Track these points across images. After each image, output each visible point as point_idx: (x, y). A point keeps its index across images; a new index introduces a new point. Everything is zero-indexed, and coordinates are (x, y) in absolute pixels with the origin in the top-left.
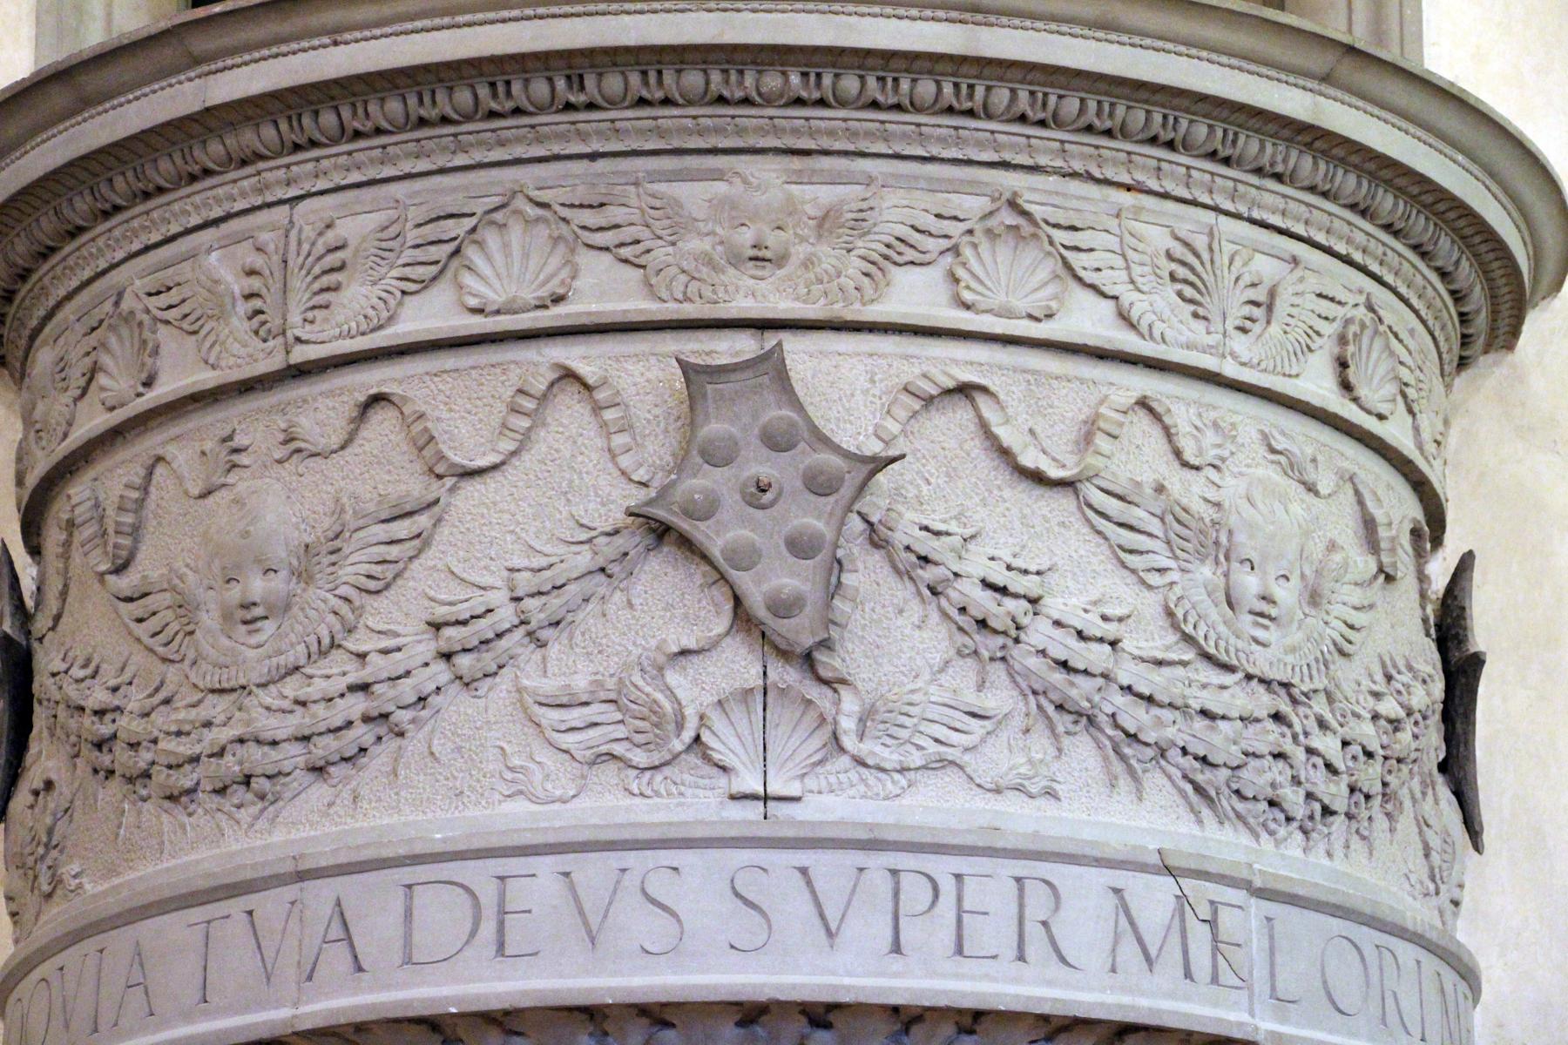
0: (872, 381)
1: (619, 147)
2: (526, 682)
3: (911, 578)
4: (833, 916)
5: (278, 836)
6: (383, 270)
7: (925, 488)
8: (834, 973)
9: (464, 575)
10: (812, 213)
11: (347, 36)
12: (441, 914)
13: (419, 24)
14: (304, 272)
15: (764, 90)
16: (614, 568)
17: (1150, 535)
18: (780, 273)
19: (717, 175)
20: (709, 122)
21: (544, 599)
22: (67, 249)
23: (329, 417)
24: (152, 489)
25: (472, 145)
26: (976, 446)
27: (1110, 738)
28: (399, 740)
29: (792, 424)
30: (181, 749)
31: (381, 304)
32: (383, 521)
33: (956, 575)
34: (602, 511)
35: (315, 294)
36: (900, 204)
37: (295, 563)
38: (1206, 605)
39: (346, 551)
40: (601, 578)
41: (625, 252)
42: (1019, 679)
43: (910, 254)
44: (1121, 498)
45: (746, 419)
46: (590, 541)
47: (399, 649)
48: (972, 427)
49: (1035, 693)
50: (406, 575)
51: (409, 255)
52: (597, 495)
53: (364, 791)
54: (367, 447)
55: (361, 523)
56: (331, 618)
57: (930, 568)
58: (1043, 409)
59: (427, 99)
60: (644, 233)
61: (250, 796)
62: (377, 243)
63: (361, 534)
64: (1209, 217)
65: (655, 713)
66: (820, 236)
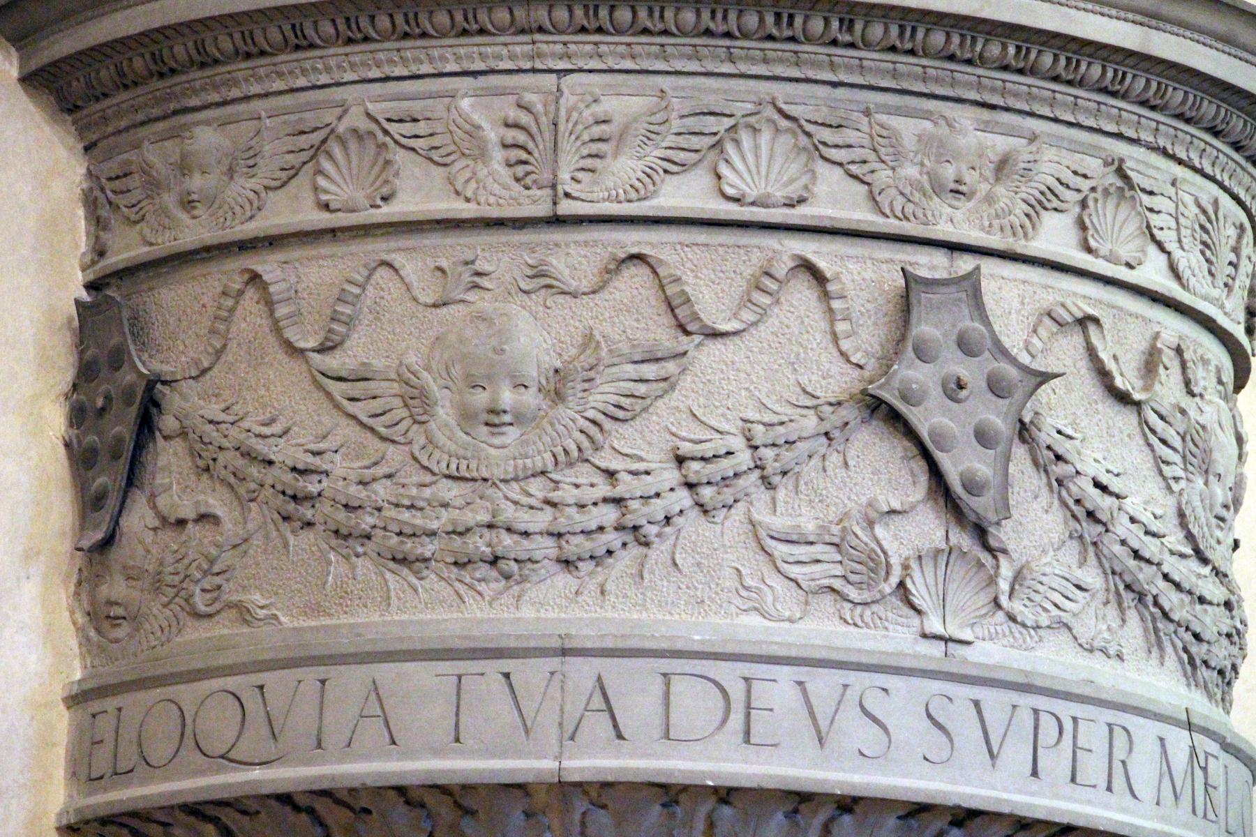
1: (860, 81)
2: (756, 517)
3: (1046, 471)
5: (527, 612)
6: (648, 149)
7: (1052, 396)
8: (994, 788)
9: (703, 419)
10: (993, 158)
12: (694, 702)
14: (573, 137)
15: (987, 55)
16: (835, 434)
18: (970, 205)
19: (927, 115)
21: (776, 450)
23: (580, 263)
24: (369, 288)
25: (741, 58)
26: (1083, 365)
27: (1152, 614)
28: (644, 550)
29: (983, 337)
32: (636, 362)
33: (1078, 472)
34: (824, 383)
35: (583, 158)
37: (544, 382)
39: (598, 381)
40: (824, 440)
41: (854, 169)
42: (1104, 560)
43: (1056, 203)
44: (1162, 418)
45: (947, 326)
46: (815, 407)
47: (647, 473)
48: (1082, 350)
49: (1114, 573)
50: (651, 410)
51: (671, 140)
52: (819, 369)
53: (610, 586)
54: (617, 295)
55: (616, 360)
56: (578, 435)
57: (1060, 464)
58: (1127, 333)
60: (871, 156)
61: (494, 574)
62: (647, 126)
63: (614, 370)
65: (872, 560)
66: (998, 179)
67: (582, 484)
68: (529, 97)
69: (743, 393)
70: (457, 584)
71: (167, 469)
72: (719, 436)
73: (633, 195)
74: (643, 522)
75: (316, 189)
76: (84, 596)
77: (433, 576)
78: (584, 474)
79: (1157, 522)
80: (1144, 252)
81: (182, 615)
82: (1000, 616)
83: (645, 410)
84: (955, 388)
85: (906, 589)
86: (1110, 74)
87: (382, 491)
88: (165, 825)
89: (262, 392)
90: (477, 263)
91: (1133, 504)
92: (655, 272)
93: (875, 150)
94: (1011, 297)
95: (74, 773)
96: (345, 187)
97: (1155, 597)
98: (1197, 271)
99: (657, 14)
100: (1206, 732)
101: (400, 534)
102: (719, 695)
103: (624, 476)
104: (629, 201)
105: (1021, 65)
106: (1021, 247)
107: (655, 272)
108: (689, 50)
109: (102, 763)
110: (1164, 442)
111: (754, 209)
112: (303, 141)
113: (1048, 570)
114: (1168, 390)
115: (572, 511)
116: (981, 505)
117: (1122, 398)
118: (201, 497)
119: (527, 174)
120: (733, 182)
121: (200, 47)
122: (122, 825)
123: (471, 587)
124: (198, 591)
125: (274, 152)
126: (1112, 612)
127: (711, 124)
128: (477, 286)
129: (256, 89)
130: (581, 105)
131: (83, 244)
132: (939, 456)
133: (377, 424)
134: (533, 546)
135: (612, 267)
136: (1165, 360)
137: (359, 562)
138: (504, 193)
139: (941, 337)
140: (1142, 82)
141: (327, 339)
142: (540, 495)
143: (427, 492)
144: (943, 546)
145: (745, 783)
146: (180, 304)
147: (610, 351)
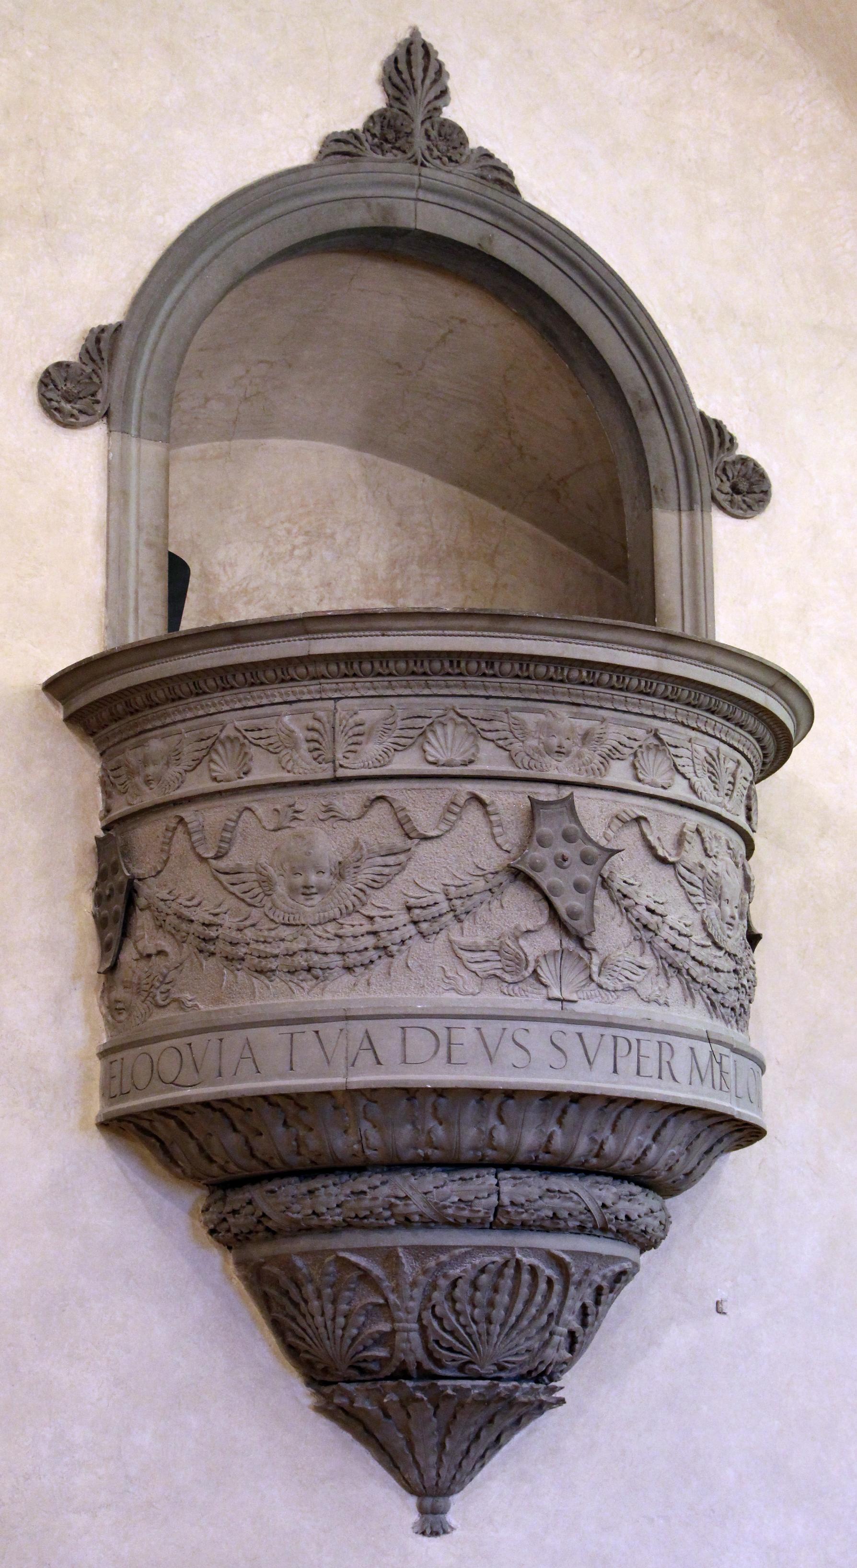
0: (601, 811)
2: (453, 938)
3: (618, 904)
4: (591, 1055)
5: (328, 997)
6: (385, 738)
7: (621, 862)
11: (389, 633)
12: (420, 1042)
13: (426, 632)
15: (571, 677)
16: (495, 890)
17: (698, 887)
18: (567, 759)
19: (541, 711)
20: (543, 688)
21: (462, 900)
22: (191, 700)
24: (240, 822)
26: (639, 844)
28: (390, 959)
30: (268, 950)
31: (384, 755)
36: (615, 734)
37: (333, 869)
38: (713, 917)
39: (362, 867)
40: (489, 893)
41: (500, 742)
43: (618, 755)
44: (689, 870)
46: (483, 876)
47: (391, 917)
48: (638, 836)
49: (661, 958)
51: (398, 733)
53: (373, 980)
55: (371, 855)
57: (626, 899)
58: (664, 827)
59: (419, 664)
60: (510, 735)
61: (309, 976)
63: (370, 860)
64: (717, 742)
66: (583, 744)
67: (356, 924)
68: (321, 714)
69: (444, 870)
70: (290, 983)
71: (142, 927)
72: (429, 894)
73: (378, 764)
74: (389, 944)
75: (210, 770)
76: (106, 998)
77: (278, 980)
78: (357, 919)
79: (688, 929)
80: (672, 779)
81: (151, 1006)
82: (593, 985)
83: (389, 882)
84: (561, 861)
85: (538, 975)
86: (643, 684)
87: (249, 934)
88: (150, 1121)
89: (188, 882)
90: (296, 806)
91: (671, 919)
92: (391, 805)
93: (512, 732)
94: (594, 810)
95: (103, 1095)
96: (224, 768)
97: (688, 970)
98: (706, 788)
99: (384, 665)
100: (719, 1042)
101: (259, 957)
102: (433, 1038)
103: (378, 919)
104: (376, 767)
105: (591, 681)
106: (598, 781)
107: (391, 805)
108: (404, 683)
109: (115, 1090)
110: (691, 884)
111: (444, 768)
112: (203, 744)
113: (621, 958)
114: (693, 854)
115: (350, 940)
116: (580, 925)
117: (663, 861)
118: (159, 942)
119: (320, 755)
120: (433, 753)
121: (148, 697)
122: (130, 1122)
123: (298, 985)
124: (158, 993)
125: (189, 751)
126: (662, 980)
127: (419, 722)
128: (296, 818)
129: (179, 717)
130: (348, 717)
131: (101, 807)
132: (554, 899)
133: (246, 897)
134: (329, 960)
135: (368, 804)
136: (688, 838)
137: (239, 973)
138: (308, 767)
139: (553, 834)
140: (663, 687)
141: (218, 852)
142: (333, 932)
143: (273, 933)
144: (559, 948)
145: (448, 1085)
146: (147, 836)
147: (368, 851)
